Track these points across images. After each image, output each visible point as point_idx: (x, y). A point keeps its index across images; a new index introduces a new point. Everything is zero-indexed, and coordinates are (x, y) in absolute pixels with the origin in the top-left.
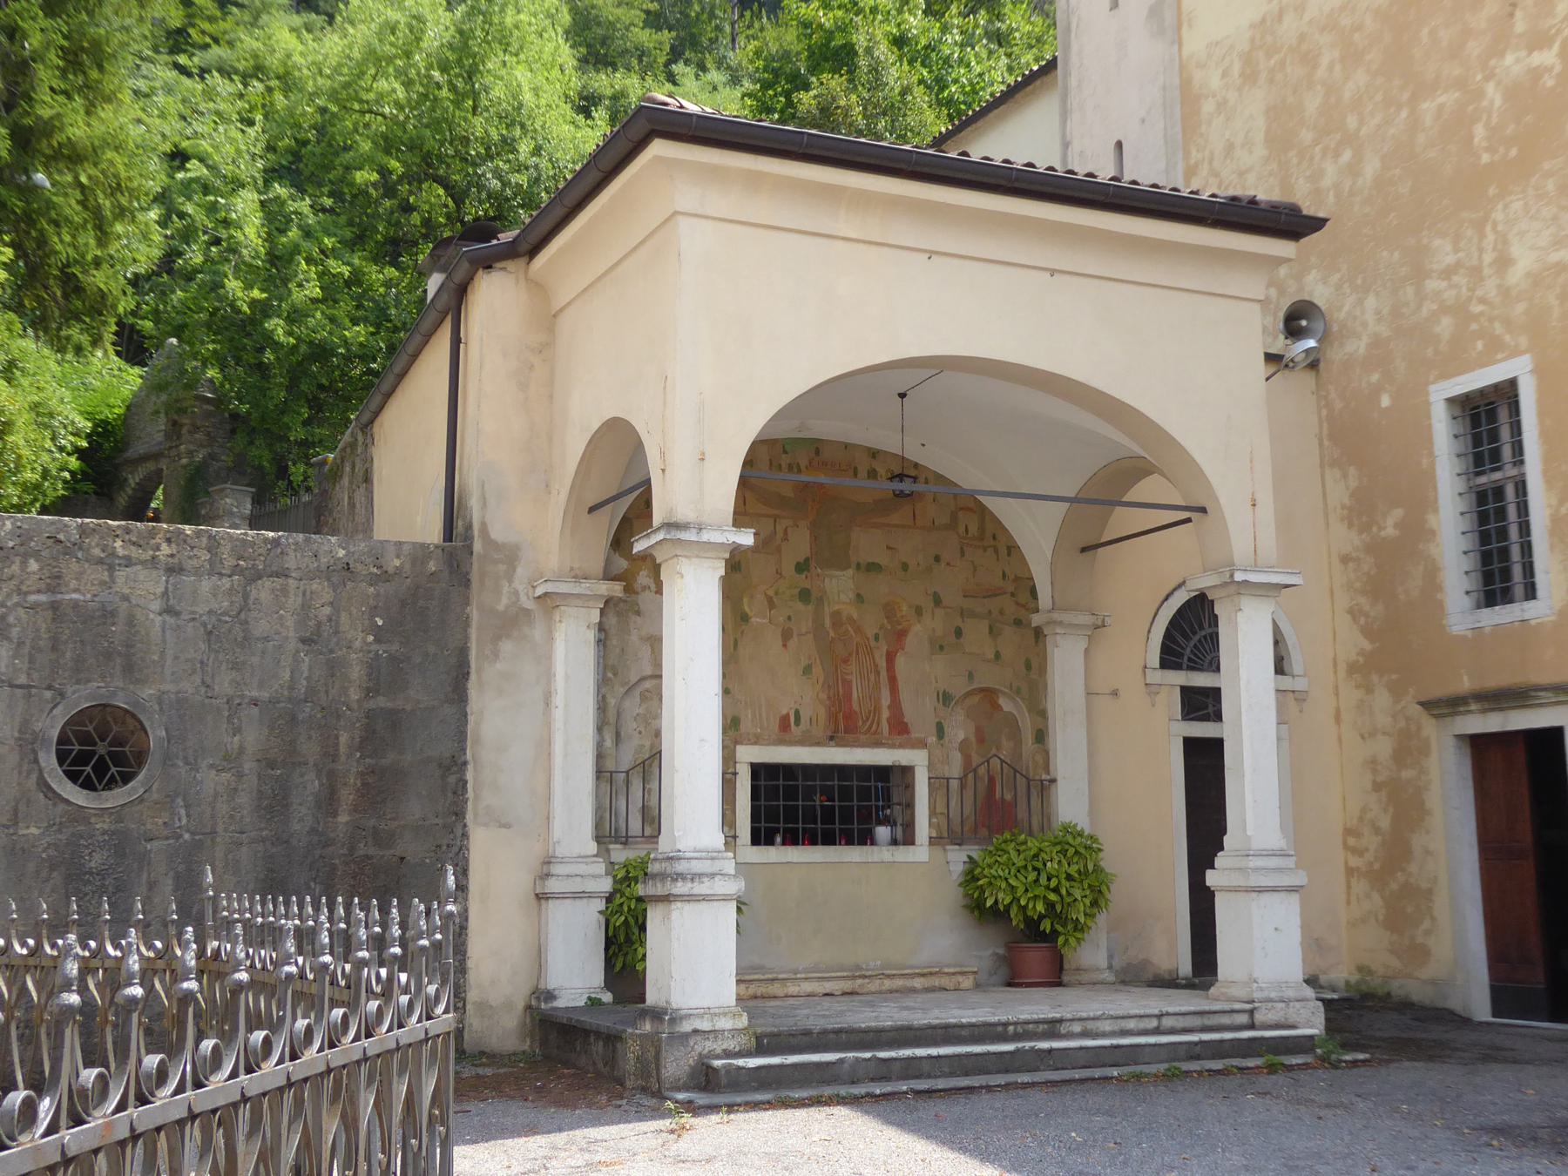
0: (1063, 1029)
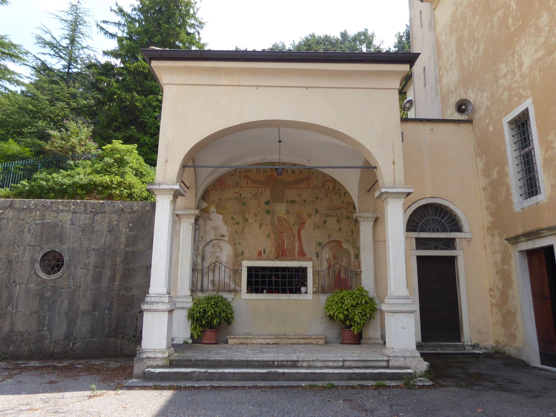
0: (299, 364)
